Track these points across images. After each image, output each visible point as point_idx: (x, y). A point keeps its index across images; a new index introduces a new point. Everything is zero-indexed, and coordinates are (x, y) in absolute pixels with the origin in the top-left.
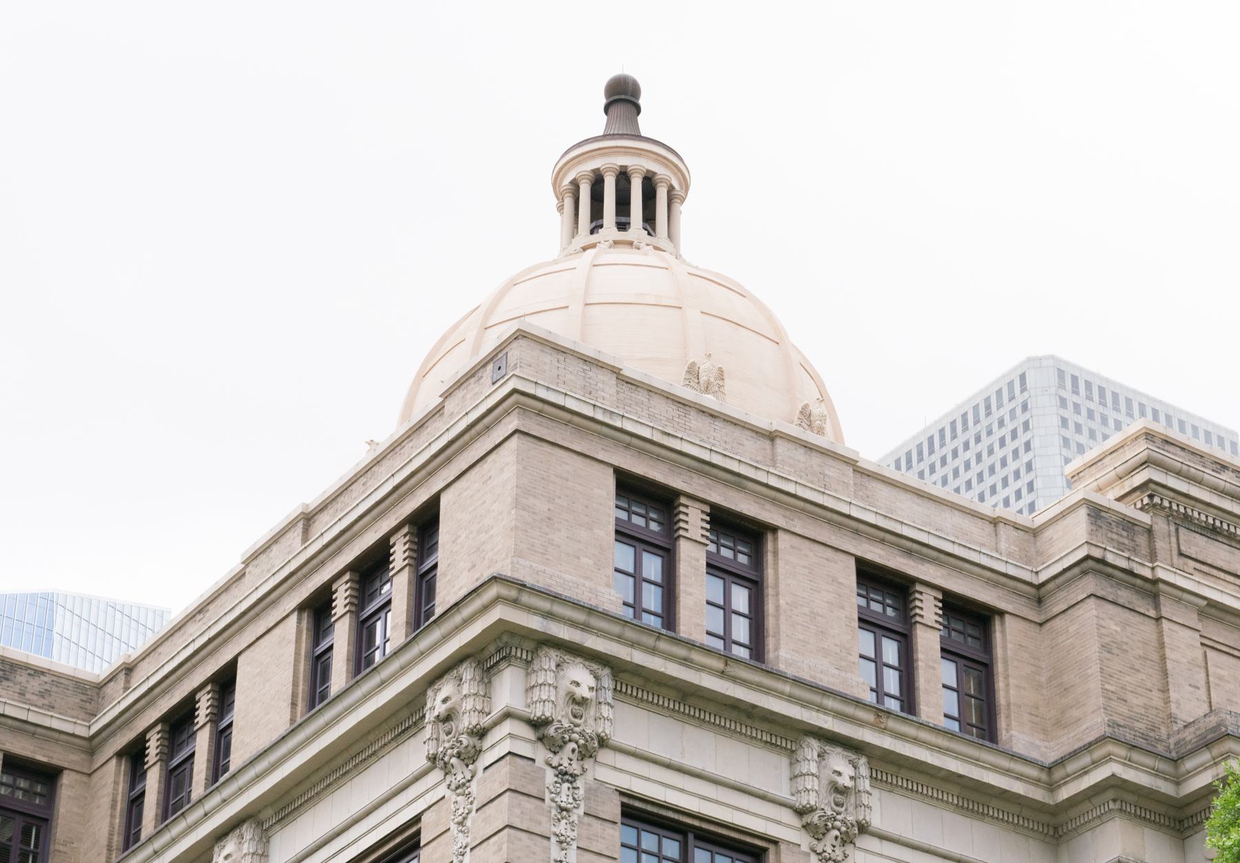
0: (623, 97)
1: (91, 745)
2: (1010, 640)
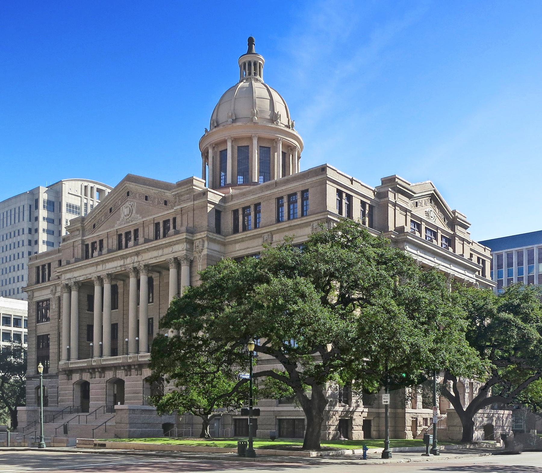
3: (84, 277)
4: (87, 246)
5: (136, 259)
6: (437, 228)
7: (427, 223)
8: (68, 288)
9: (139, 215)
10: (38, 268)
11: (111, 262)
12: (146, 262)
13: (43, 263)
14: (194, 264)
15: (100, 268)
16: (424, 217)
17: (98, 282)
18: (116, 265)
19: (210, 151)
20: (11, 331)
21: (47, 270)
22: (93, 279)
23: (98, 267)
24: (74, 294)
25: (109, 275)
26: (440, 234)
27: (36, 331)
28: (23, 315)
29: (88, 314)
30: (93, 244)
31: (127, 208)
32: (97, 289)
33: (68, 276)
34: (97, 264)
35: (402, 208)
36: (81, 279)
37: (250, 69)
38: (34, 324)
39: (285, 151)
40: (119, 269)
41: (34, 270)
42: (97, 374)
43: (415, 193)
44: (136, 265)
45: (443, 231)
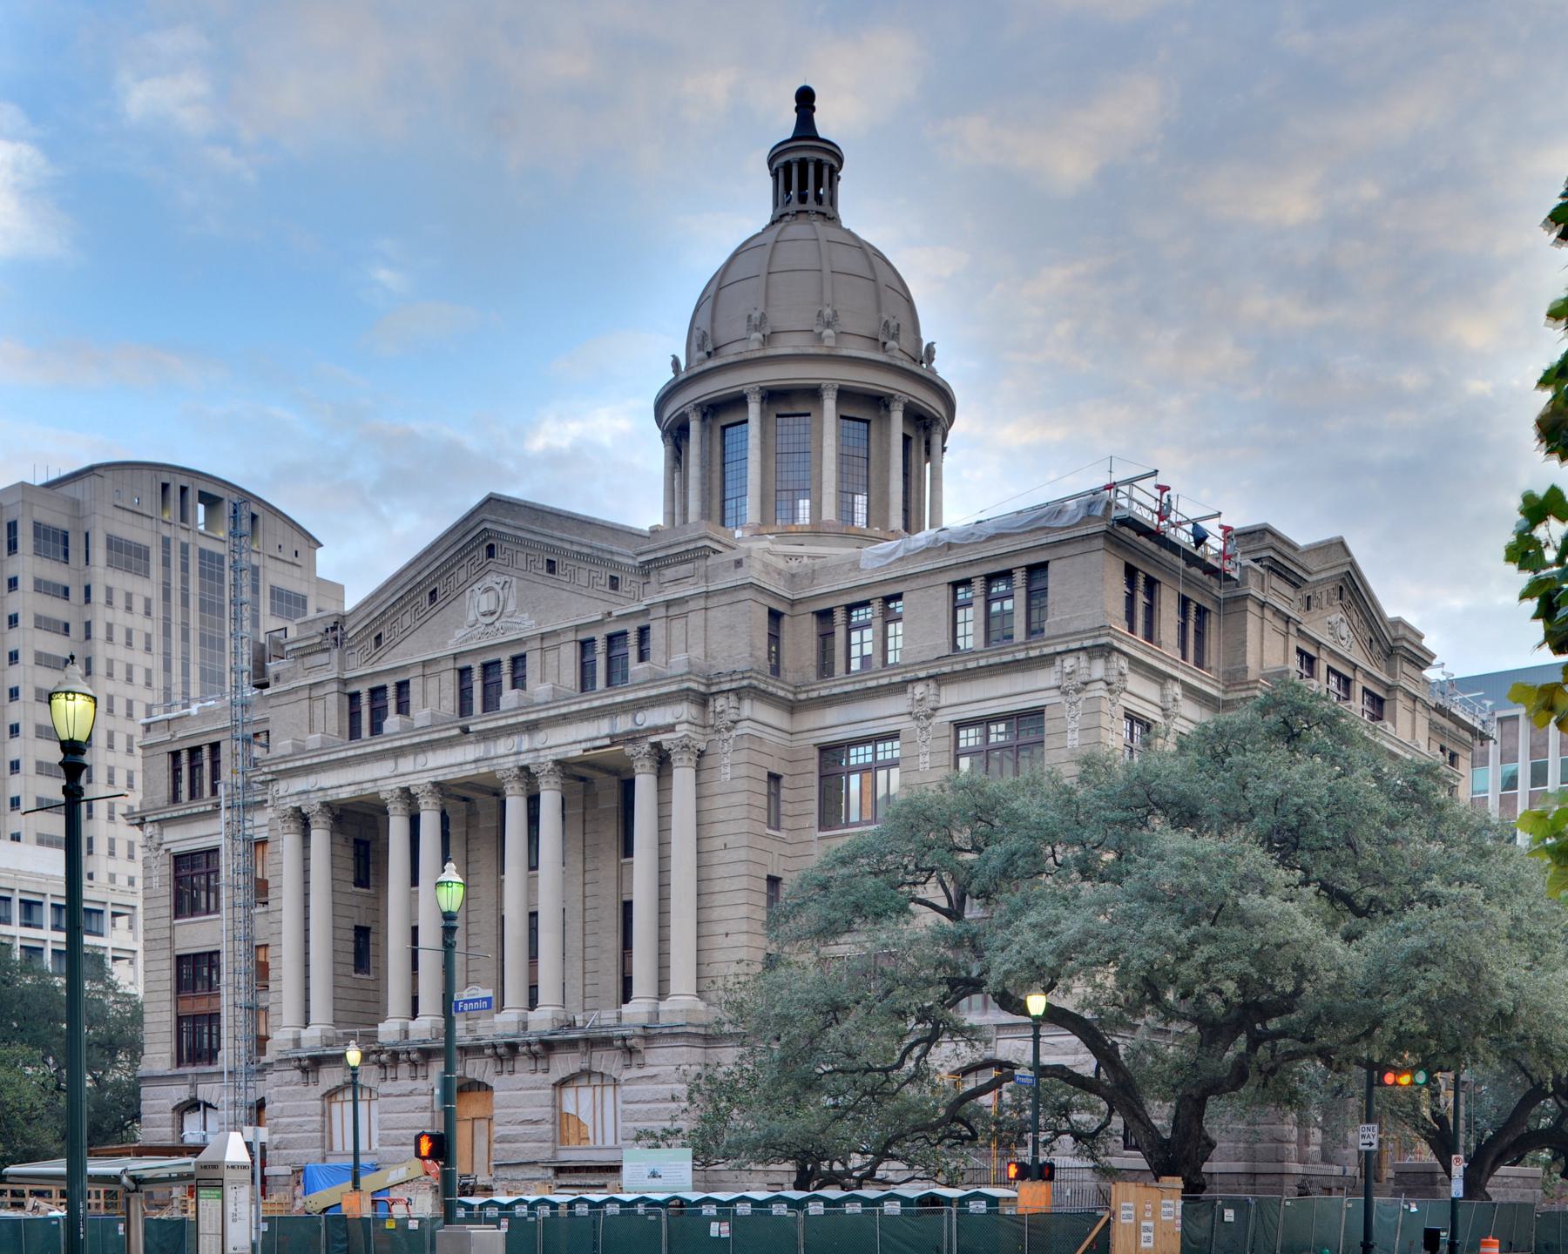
0: (805, 99)
1: (793, 603)
2: (863, 426)
3: (353, 788)
4: (354, 697)
5: (525, 742)
6: (1355, 667)
7: (1332, 653)
8: (303, 822)
9: (526, 615)
10: (176, 755)
11: (444, 748)
12: (560, 754)
13: (194, 743)
14: (708, 761)
15: (406, 764)
16: (1326, 639)
17: (400, 806)
18: (460, 759)
19: (694, 426)
20: (13, 937)
21: (207, 764)
22: (382, 796)
23: (401, 761)
24: (320, 838)
25: (439, 787)
26: (1359, 684)
27: (171, 939)
28: (49, 890)
29: (357, 894)
30: (377, 693)
31: (487, 590)
32: (397, 828)
33: (300, 784)
34: (397, 753)
35: (1277, 612)
36: (344, 794)
37: (803, 185)
38: (166, 922)
39: (910, 433)
40: (470, 770)
41: (164, 763)
42: (404, 1069)
43: (1310, 573)
44: (526, 760)
45: (1368, 675)
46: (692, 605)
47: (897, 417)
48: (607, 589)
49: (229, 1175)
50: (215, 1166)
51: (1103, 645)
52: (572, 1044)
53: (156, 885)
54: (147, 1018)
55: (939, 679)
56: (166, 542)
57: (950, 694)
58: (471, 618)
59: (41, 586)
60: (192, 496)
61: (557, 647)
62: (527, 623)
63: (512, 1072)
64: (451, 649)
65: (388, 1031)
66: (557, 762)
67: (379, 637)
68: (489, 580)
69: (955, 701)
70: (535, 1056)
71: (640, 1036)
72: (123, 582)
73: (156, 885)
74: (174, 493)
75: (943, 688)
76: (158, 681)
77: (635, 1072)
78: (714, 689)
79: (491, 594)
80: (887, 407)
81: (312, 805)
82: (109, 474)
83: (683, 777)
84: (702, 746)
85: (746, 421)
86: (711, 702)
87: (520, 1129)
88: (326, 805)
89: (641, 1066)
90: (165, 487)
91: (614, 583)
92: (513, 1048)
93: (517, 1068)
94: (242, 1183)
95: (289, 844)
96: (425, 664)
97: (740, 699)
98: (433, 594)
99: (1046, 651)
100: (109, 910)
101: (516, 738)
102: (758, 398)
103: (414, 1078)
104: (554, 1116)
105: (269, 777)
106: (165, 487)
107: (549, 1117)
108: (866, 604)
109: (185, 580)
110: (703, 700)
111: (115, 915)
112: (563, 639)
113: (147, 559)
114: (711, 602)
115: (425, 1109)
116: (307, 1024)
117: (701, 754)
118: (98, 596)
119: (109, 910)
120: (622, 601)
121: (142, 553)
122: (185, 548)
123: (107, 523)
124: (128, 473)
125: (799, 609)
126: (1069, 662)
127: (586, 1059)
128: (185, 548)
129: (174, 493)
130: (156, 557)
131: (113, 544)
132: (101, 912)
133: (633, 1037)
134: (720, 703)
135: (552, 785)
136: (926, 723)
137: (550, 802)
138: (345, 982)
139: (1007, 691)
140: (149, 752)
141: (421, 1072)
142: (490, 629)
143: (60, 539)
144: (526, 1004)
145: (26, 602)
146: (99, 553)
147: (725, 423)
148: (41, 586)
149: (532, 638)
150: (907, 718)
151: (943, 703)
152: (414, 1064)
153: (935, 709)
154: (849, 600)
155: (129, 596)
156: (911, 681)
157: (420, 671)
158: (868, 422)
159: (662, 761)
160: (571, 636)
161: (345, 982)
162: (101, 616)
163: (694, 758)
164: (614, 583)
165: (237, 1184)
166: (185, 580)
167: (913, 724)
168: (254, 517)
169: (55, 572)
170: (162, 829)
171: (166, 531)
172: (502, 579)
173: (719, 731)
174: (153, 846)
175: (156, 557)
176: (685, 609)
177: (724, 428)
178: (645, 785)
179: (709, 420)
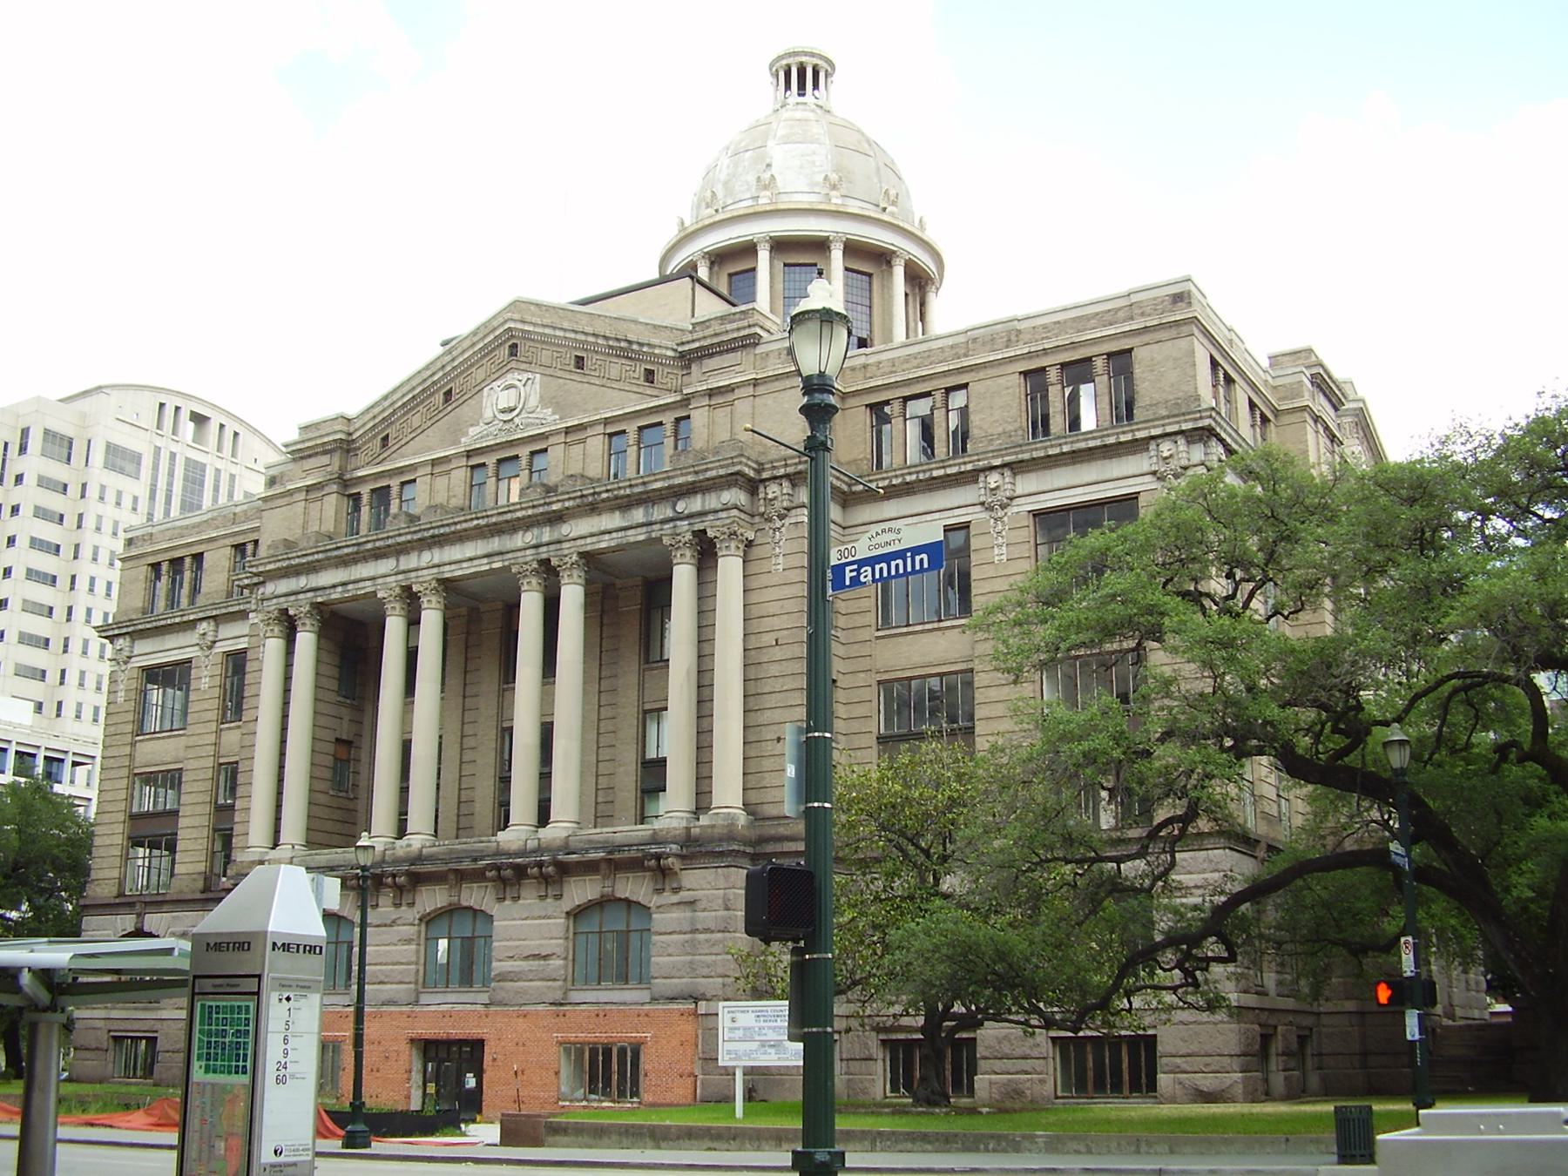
5: (546, 534)
14: (756, 552)
23: (402, 558)
24: (306, 641)
32: (394, 628)
41: (143, 571)
44: (544, 553)
46: (738, 393)
47: (899, 272)
48: (641, 381)
49: (274, 967)
50: (242, 944)
51: (1202, 428)
52: (590, 868)
53: (120, 700)
54: (97, 841)
55: (1017, 468)
56: (158, 450)
57: (1026, 483)
58: (488, 414)
59: (44, 482)
60: (185, 415)
61: (583, 441)
62: (550, 419)
63: (516, 899)
64: (466, 443)
65: (378, 838)
66: (582, 555)
67: (386, 438)
68: (511, 378)
69: (1033, 489)
70: (545, 880)
71: (677, 856)
72: (114, 481)
73: (120, 700)
74: (169, 412)
75: (1019, 478)
76: (143, 506)
77: (669, 898)
78: (765, 475)
79: (512, 391)
80: (889, 264)
81: (299, 608)
82: (115, 392)
83: (730, 568)
84: (751, 535)
85: (754, 269)
86: (761, 489)
87: (524, 965)
88: (317, 607)
89: (676, 890)
90: (162, 405)
91: (649, 376)
92: (520, 872)
93: (523, 894)
94: (305, 987)
95: (273, 647)
96: (434, 463)
97: (794, 486)
98: (448, 394)
99: (1139, 435)
100: (70, 759)
101: (536, 531)
102: (767, 246)
103: (397, 905)
104: (567, 950)
105: (255, 580)
106: (162, 405)
107: (559, 951)
108: (928, 394)
109: (170, 484)
110: (753, 486)
111: (75, 764)
112: (590, 432)
113: (139, 464)
114: (761, 390)
115: (408, 941)
116: (275, 845)
117: (749, 544)
118: (93, 492)
119: (70, 759)
120: (655, 392)
121: (136, 458)
122: (173, 456)
123: (108, 431)
124: (131, 392)
125: (852, 402)
126: (1166, 448)
127: (608, 883)
128: (173, 456)
129: (169, 412)
130: (147, 462)
131: (111, 449)
132: (62, 761)
133: (668, 856)
134: (773, 490)
135: (575, 579)
136: (1001, 513)
137: (572, 597)
138: (323, 799)
139: (1093, 478)
140: (129, 564)
141: (407, 898)
142: (507, 426)
143: (66, 444)
144: (534, 821)
145: (29, 495)
146: (98, 457)
147: (732, 270)
148: (44, 482)
149: (556, 433)
150: (978, 508)
151: (1019, 491)
152: (400, 889)
153: (1011, 499)
154: (907, 392)
155: (119, 494)
156: (983, 470)
157: (428, 469)
158: (870, 275)
159: (706, 553)
160: (600, 429)
161: (323, 799)
162: (92, 508)
163: (742, 546)
164: (649, 376)
165: (294, 987)
166: (170, 484)
167: (985, 515)
168: (236, 434)
169: (58, 471)
170: (133, 641)
171: (159, 442)
172: (525, 376)
173: (770, 520)
174: (121, 660)
175: (147, 462)
176: (730, 397)
177: (730, 275)
178: (683, 577)
179: (716, 268)
